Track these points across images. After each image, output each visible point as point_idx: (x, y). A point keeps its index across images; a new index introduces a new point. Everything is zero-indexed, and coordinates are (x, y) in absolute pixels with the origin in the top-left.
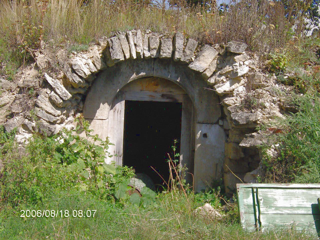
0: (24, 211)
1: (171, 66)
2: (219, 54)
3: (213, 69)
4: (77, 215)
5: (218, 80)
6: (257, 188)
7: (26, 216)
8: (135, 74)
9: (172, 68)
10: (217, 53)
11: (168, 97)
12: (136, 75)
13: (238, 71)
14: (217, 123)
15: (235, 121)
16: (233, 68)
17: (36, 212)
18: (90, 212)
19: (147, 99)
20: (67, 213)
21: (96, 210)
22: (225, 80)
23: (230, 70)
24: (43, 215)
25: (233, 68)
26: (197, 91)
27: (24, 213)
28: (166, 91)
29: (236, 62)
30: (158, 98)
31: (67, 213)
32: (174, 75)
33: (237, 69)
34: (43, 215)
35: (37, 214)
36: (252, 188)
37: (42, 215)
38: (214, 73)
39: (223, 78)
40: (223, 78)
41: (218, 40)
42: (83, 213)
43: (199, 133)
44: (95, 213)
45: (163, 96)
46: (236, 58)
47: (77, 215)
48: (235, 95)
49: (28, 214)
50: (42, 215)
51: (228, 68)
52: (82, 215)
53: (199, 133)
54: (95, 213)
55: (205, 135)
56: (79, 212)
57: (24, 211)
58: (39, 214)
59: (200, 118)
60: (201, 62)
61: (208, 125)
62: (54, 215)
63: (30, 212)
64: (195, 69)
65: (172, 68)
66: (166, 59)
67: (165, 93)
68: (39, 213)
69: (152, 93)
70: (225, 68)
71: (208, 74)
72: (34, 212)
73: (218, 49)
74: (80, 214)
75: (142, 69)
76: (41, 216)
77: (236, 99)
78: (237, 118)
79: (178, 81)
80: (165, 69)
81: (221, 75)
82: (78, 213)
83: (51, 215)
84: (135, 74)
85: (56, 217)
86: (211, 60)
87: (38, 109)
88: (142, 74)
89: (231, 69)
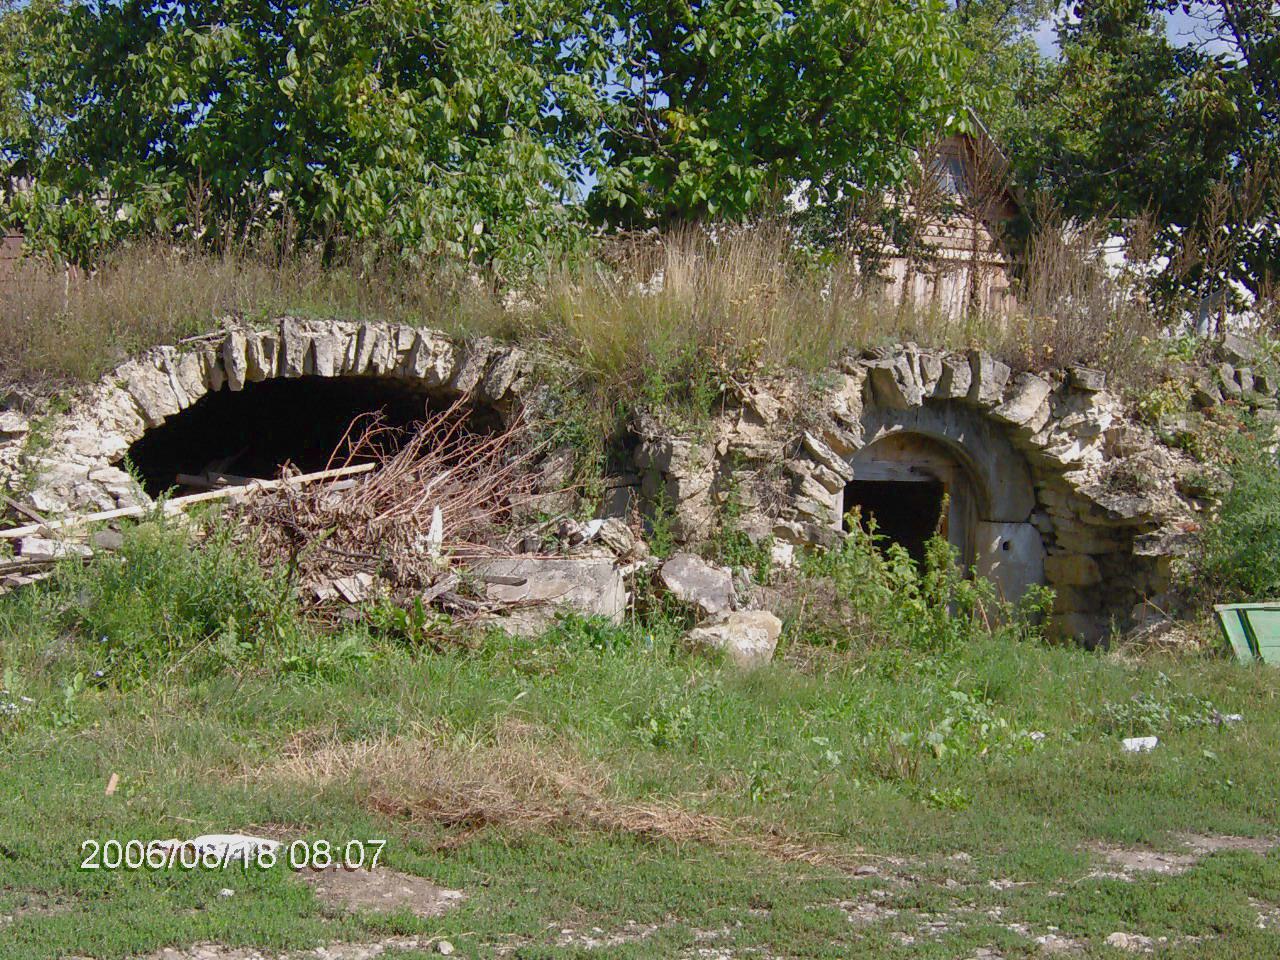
0: (96, 844)
1: (948, 412)
2: (1052, 392)
3: (1044, 419)
4: (307, 860)
5: (1055, 440)
6: (1245, 611)
7: (102, 864)
8: (883, 429)
9: (949, 416)
10: (1049, 389)
11: (924, 473)
12: (886, 430)
13: (1100, 422)
14: (1028, 521)
15: (1114, 512)
16: (1086, 417)
17: (146, 849)
18: (361, 847)
19: (883, 477)
20: (322, 853)
21: (384, 842)
22: (1068, 440)
23: (1080, 421)
24: (172, 860)
25: (1086, 417)
26: (994, 460)
27: (96, 852)
28: (919, 460)
29: (1092, 406)
30: (904, 476)
31: (270, 853)
32: (953, 429)
33: (1096, 420)
34: (172, 860)
35: (149, 854)
36: (1238, 610)
37: (168, 861)
38: (1045, 427)
39: (1064, 435)
40: (1064, 435)
41: (1047, 362)
42: (334, 853)
43: (997, 541)
44: (379, 851)
45: (913, 470)
46: (1094, 398)
47: (307, 860)
48: (1085, 466)
49: (135, 855)
50: (168, 861)
51: (1076, 418)
52: (329, 860)
53: (997, 541)
54: (379, 851)
55: (1006, 546)
56: (315, 848)
57: (96, 844)
58: (154, 855)
59: (998, 512)
60: (1022, 406)
61: (1014, 525)
62: (215, 861)
63: (119, 847)
64: (1012, 419)
65: (949, 416)
66: (956, 401)
67: (916, 465)
68: (157, 851)
69: (890, 464)
70: (1070, 418)
71: (1036, 428)
72: (113, 848)
73: (1050, 383)
74: (322, 858)
75: (896, 418)
76: (162, 864)
77: (1088, 475)
78: (1116, 508)
79: (960, 440)
80: (938, 418)
81: (1059, 430)
82: (312, 852)
83: (205, 861)
84: (883, 429)
85: (225, 866)
86: (1038, 402)
87: (805, 499)
88: (897, 427)
89: (1082, 418)
